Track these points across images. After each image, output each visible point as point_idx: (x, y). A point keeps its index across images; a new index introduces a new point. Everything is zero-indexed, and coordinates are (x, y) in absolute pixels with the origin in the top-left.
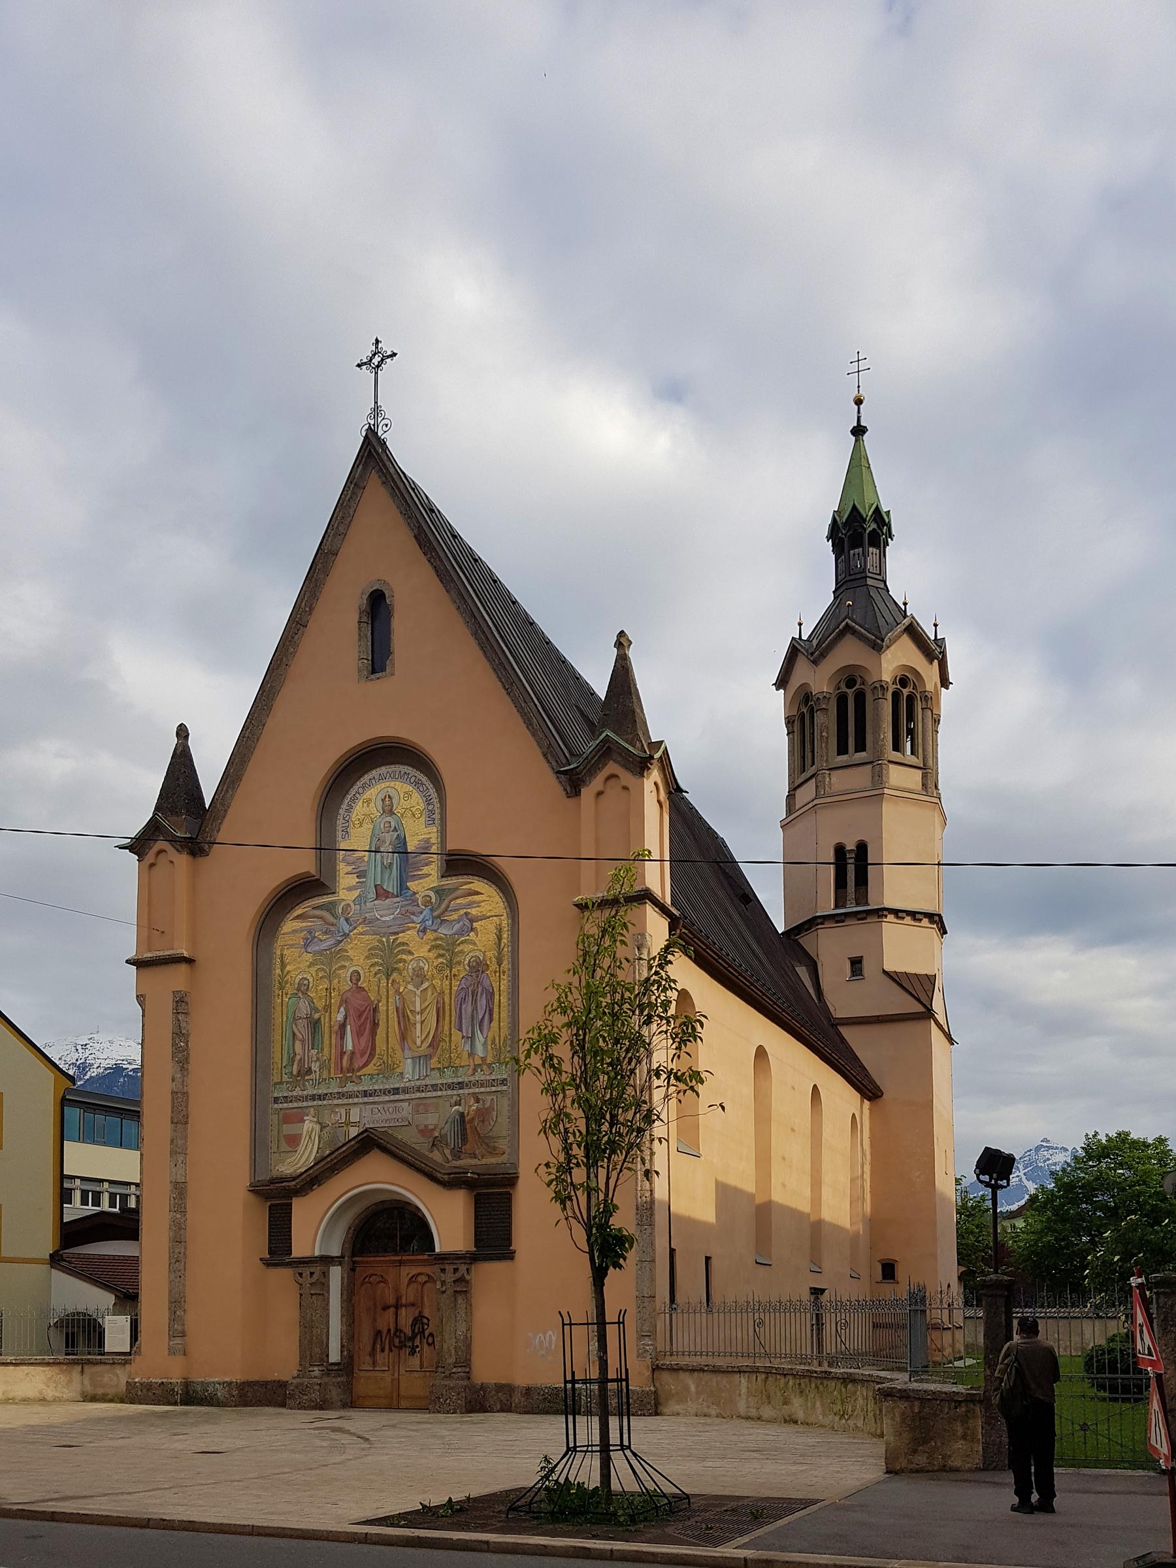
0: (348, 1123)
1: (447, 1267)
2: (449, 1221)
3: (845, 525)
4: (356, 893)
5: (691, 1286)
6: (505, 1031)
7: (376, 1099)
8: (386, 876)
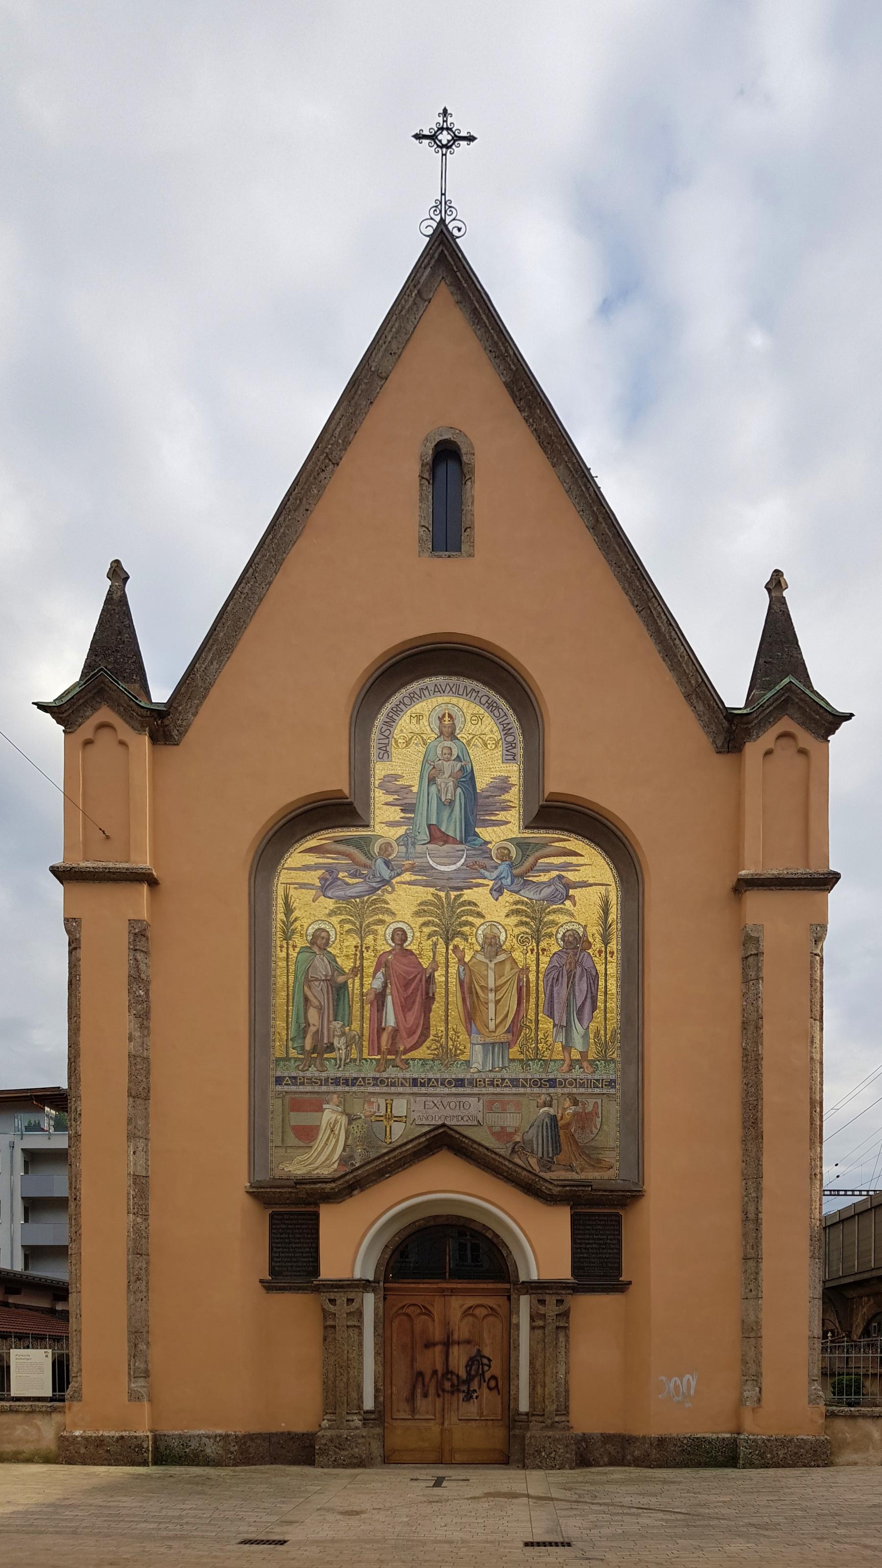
0: (390, 1117)
1: (547, 1298)
2: (542, 1243)
4: (401, 831)
7: (431, 1090)
8: (446, 814)
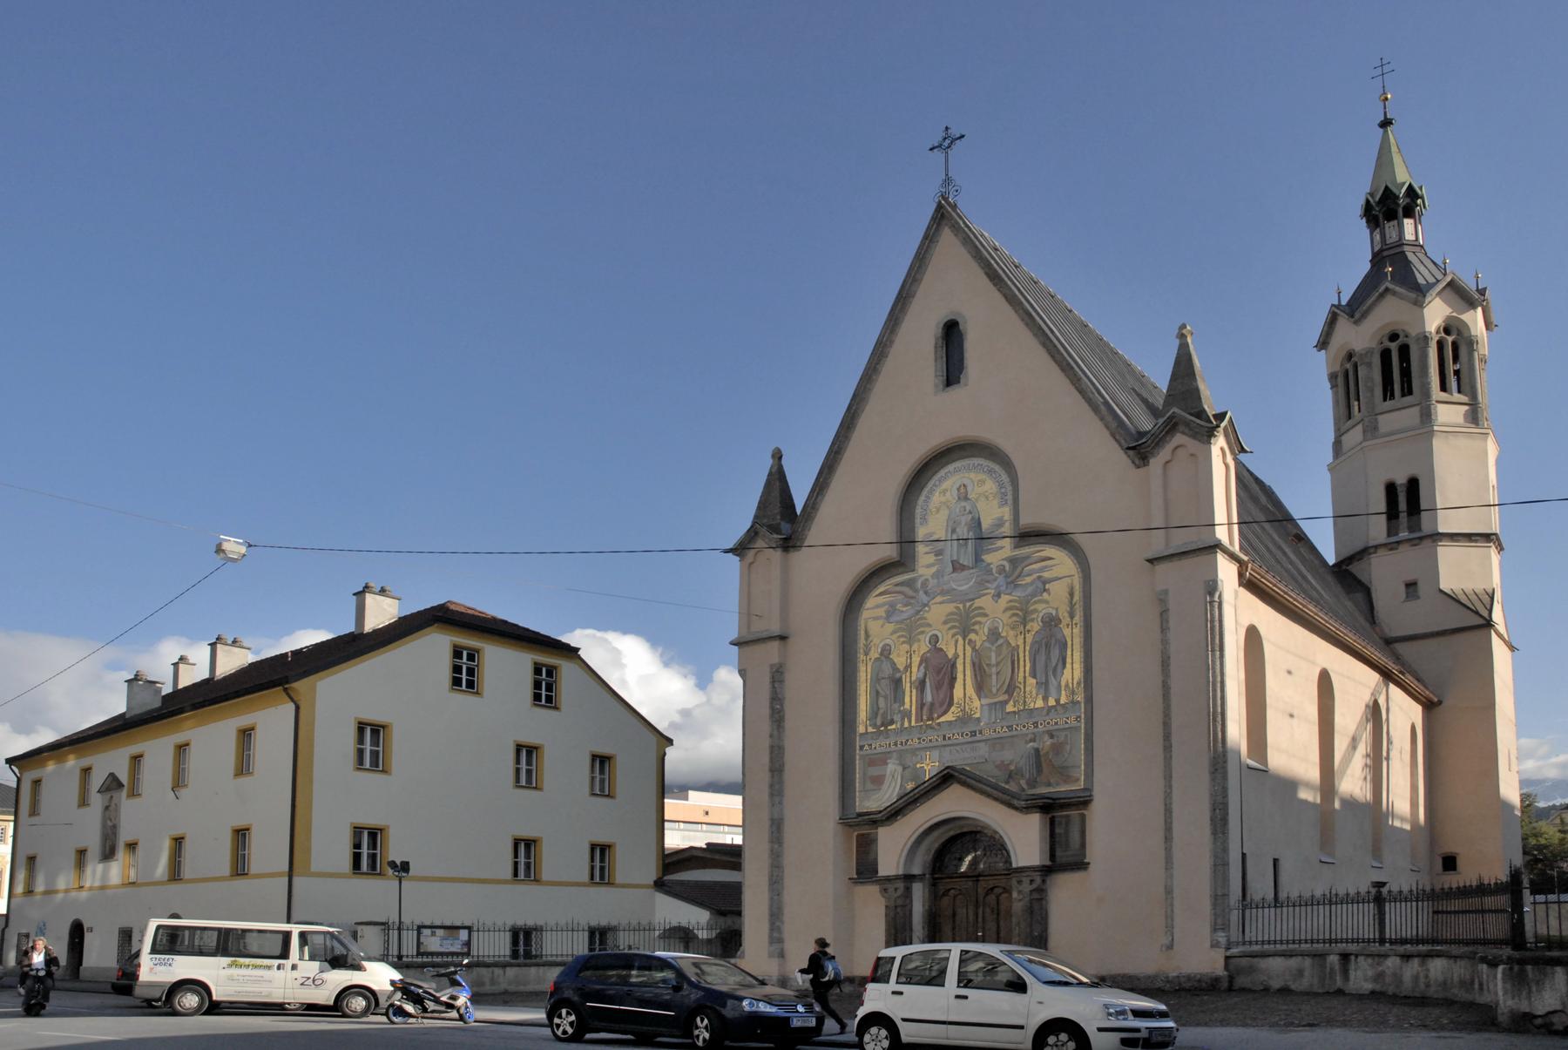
4: (934, 569)
5: (1261, 887)
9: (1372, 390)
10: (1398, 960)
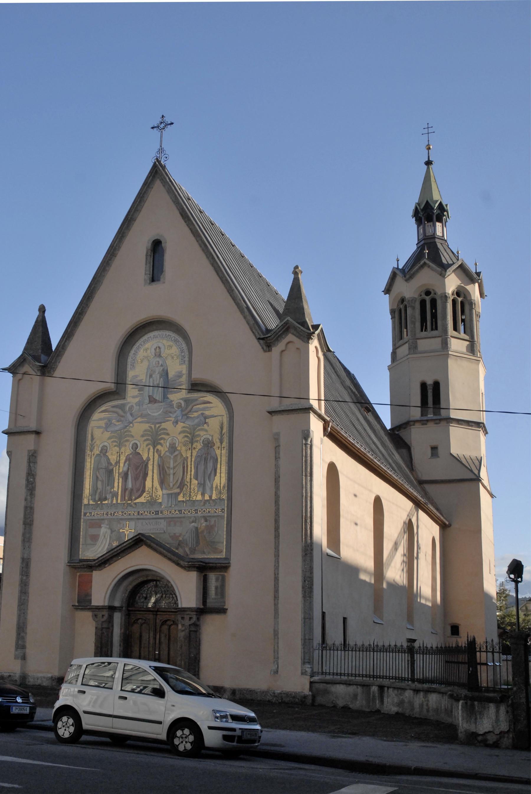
1: (185, 616)
3: (422, 210)
4: (137, 400)
5: (335, 636)
6: (224, 480)
9: (414, 323)
10: (411, 692)
